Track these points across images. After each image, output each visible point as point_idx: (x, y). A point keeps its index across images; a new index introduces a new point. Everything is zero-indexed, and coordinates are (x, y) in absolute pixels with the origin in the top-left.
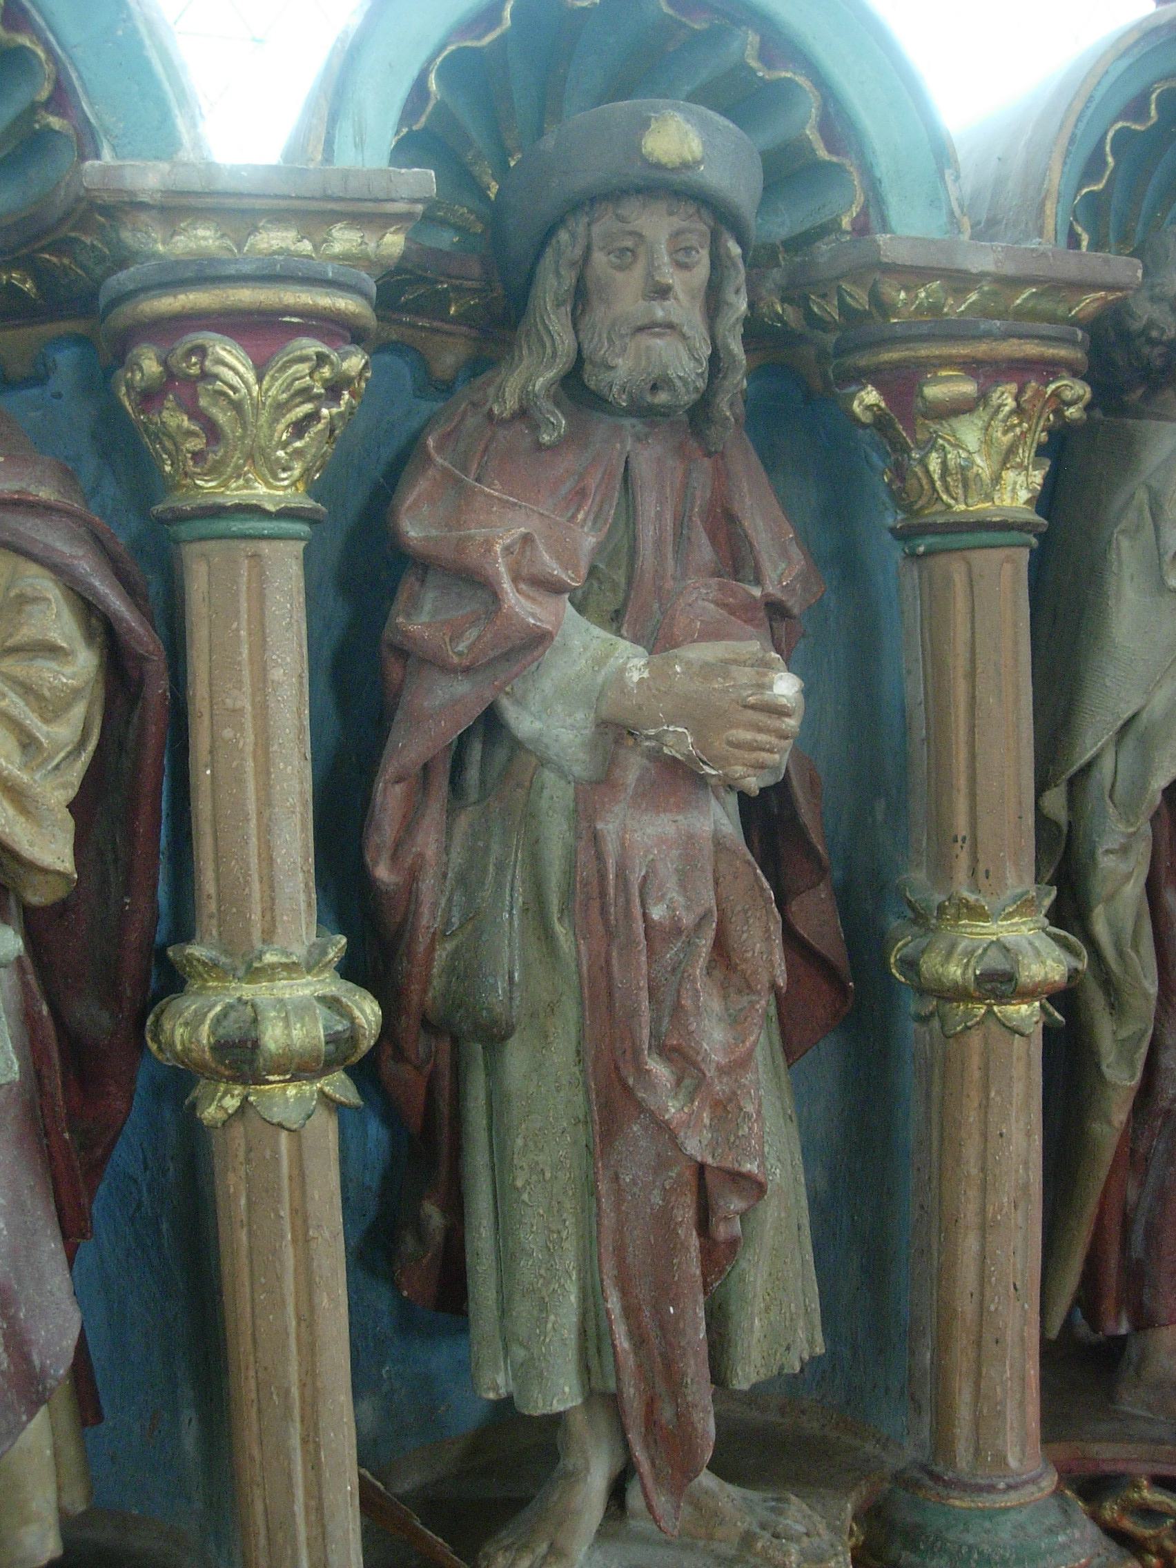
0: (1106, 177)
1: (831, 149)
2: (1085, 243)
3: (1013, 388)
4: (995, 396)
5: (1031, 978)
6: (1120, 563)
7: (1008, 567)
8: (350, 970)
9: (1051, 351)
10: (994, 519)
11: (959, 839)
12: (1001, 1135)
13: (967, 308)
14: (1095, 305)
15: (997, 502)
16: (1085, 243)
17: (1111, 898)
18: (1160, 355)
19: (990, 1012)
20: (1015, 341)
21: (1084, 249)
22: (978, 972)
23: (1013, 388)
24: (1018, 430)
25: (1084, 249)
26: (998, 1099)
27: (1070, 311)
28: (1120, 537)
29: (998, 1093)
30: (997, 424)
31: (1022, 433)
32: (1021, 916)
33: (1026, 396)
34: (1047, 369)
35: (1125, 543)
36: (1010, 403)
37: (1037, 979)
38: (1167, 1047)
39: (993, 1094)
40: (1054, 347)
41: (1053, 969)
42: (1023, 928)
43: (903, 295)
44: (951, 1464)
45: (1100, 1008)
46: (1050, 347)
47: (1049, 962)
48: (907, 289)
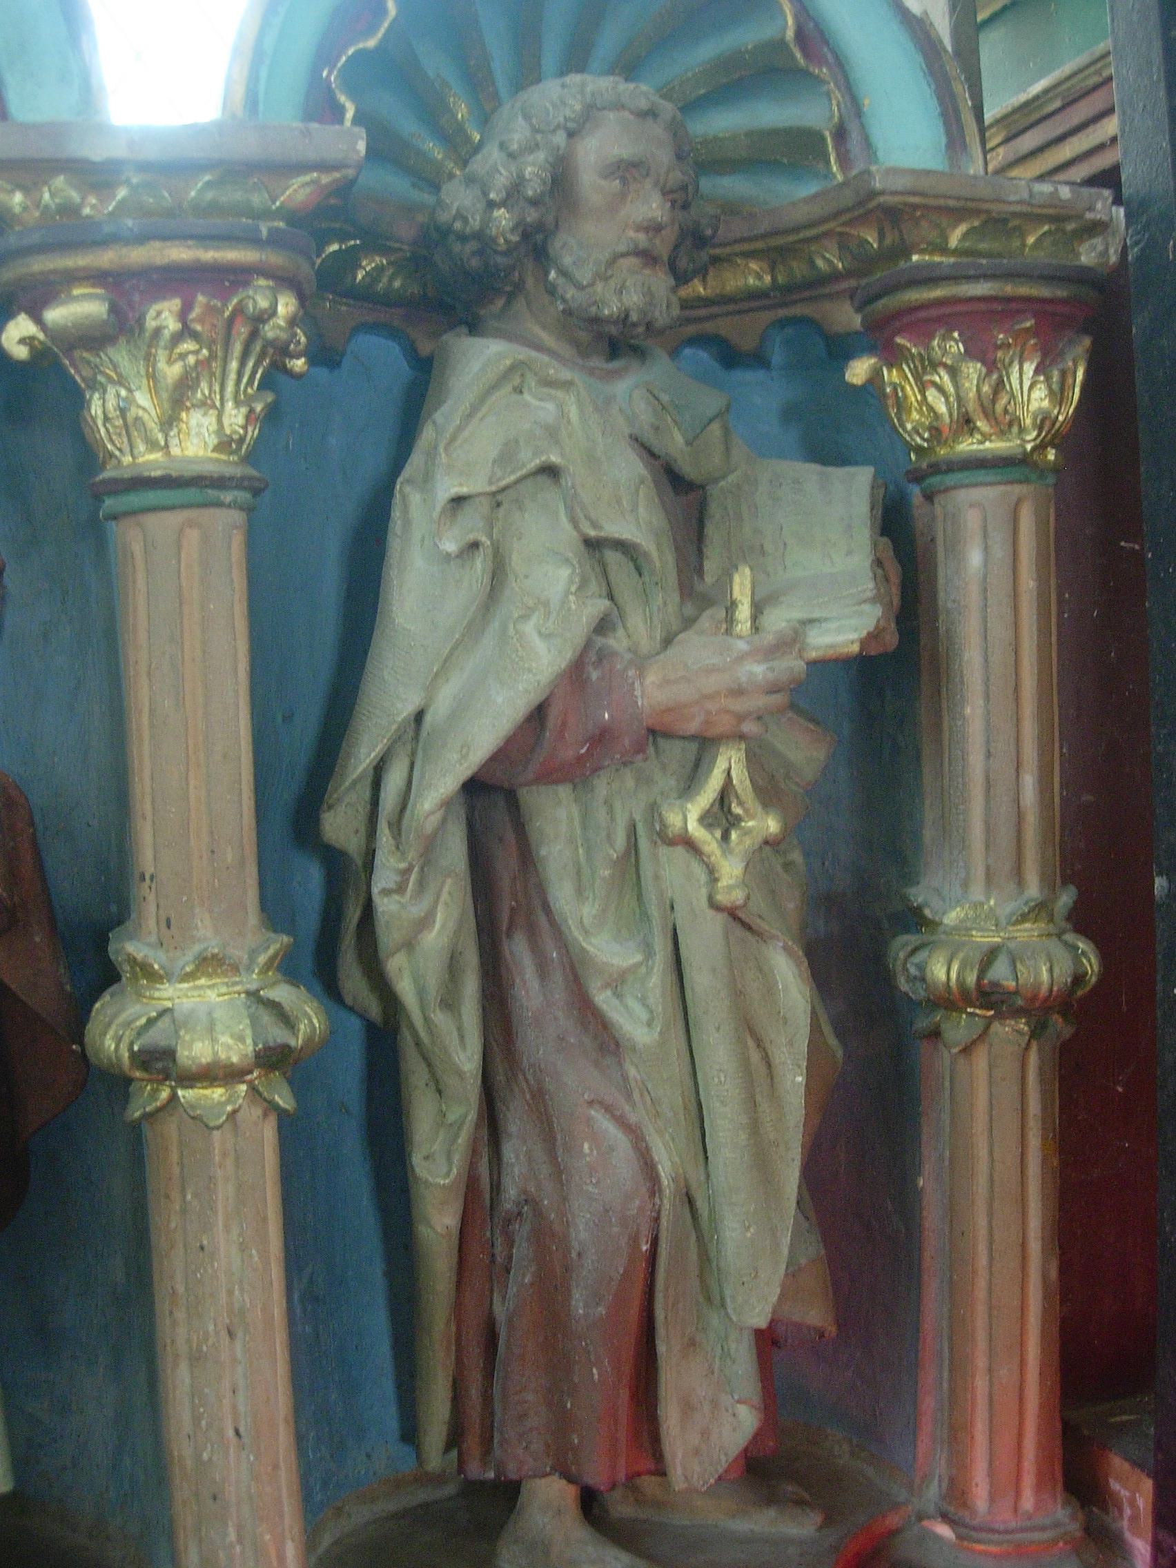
0: (383, 30)
1: (807, 55)
2: (350, 114)
3: (176, 304)
4: (152, 313)
5: (193, 1059)
6: (407, 523)
7: (193, 536)
8: (287, 968)
9: (232, 255)
10: (153, 474)
11: (147, 877)
12: (202, 1248)
13: (116, 208)
14: (308, 190)
15: (175, 451)
16: (350, 114)
17: (409, 945)
18: (473, 254)
19: (174, 1097)
20: (157, 244)
21: (348, 123)
22: (136, 1048)
23: (176, 304)
24: (191, 360)
25: (348, 123)
26: (195, 1203)
27: (274, 202)
28: (408, 489)
29: (195, 1195)
30: (162, 355)
31: (198, 362)
32: (210, 976)
33: (193, 315)
34: (239, 276)
35: (415, 498)
36: (172, 325)
37: (204, 1061)
38: (510, 1135)
39: (189, 1197)
40: (217, 248)
41: (229, 1047)
42: (209, 992)
43: (18, 197)
44: (974, 1513)
45: (422, 1084)
46: (206, 249)
47: (225, 1039)
48: (26, 190)
